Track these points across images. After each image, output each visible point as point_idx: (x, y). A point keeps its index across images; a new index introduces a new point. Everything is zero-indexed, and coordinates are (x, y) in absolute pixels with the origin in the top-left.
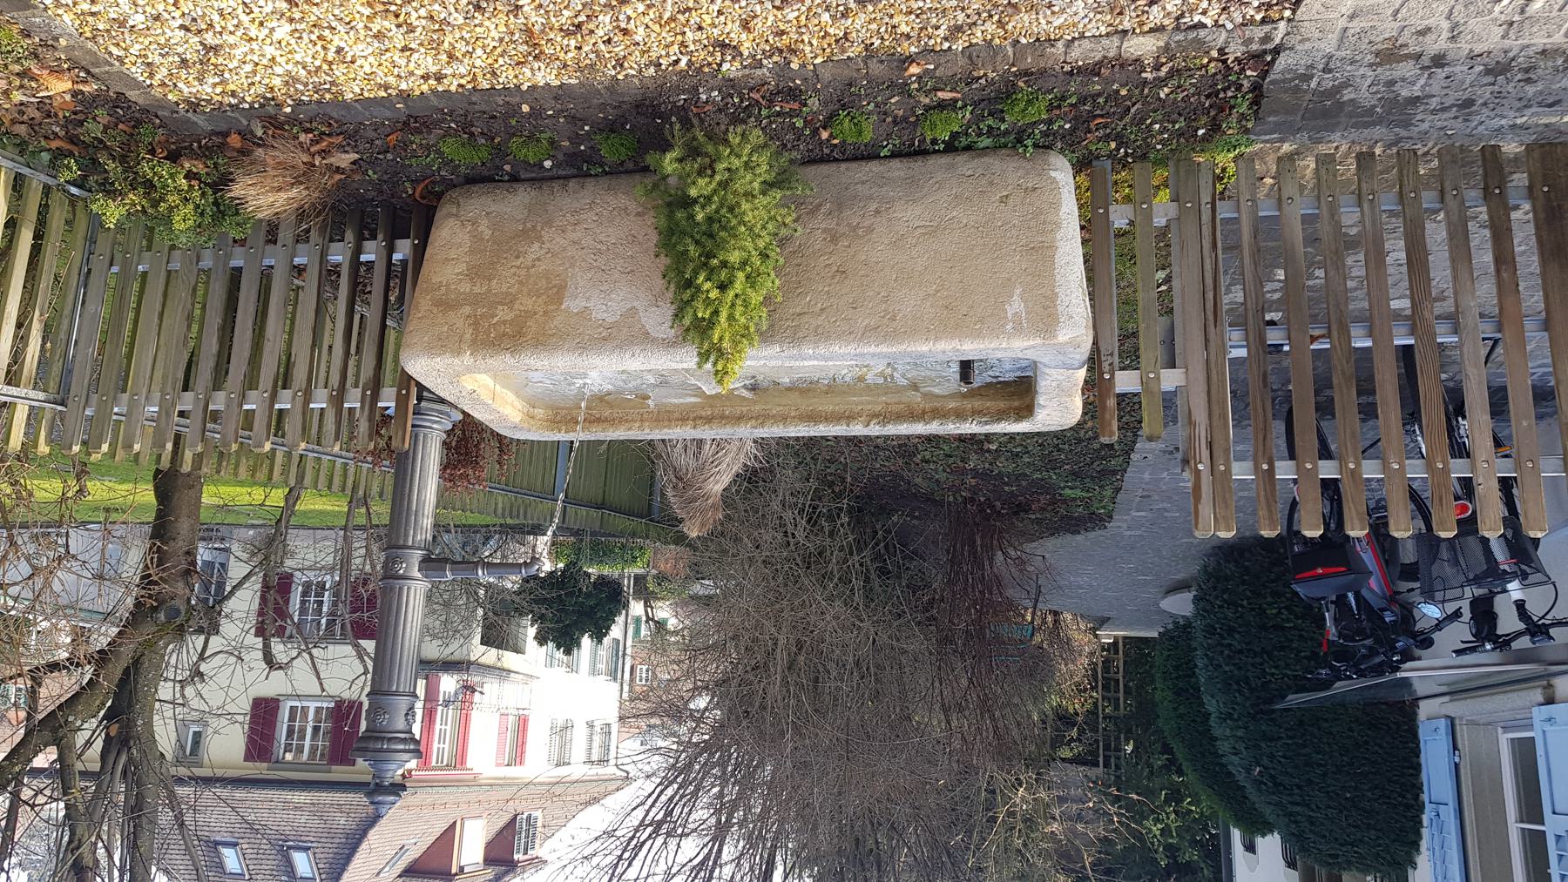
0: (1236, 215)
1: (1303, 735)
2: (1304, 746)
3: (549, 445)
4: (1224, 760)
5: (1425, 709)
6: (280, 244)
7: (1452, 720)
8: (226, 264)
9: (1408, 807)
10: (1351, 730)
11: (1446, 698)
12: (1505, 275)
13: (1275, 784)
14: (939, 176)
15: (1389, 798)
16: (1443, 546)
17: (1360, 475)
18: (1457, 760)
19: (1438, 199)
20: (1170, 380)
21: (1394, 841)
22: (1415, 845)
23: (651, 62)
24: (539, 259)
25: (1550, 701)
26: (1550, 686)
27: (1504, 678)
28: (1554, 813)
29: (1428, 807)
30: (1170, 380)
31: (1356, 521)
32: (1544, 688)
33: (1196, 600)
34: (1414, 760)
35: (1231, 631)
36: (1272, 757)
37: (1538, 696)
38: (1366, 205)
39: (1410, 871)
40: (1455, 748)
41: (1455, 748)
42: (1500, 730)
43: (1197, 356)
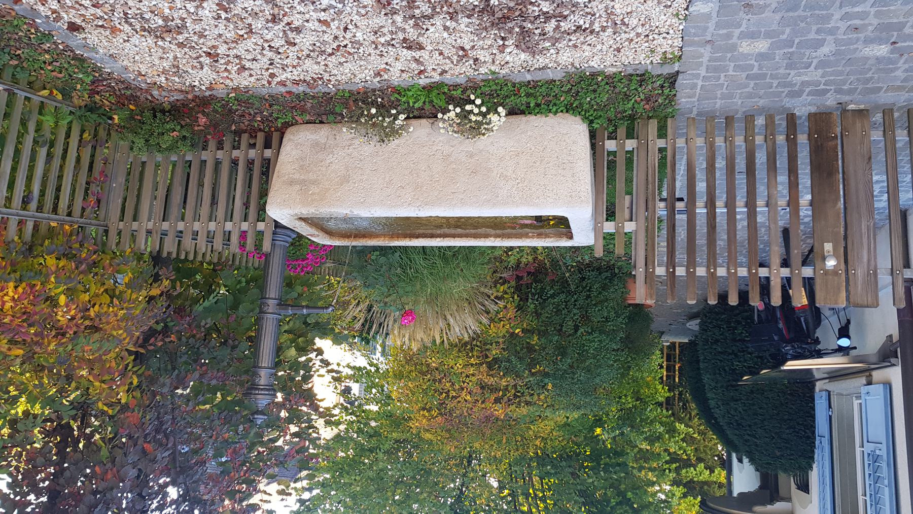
0: (666, 146)
1: (753, 399)
2: (754, 405)
3: (336, 248)
4: (713, 411)
5: (819, 385)
6: (209, 150)
7: (829, 392)
8: (183, 159)
9: (808, 437)
10: (778, 396)
11: (827, 381)
12: (792, 178)
13: (738, 425)
14: (522, 126)
15: (798, 433)
16: (31, 416)
17: (716, 275)
18: (830, 413)
19: (764, 139)
20: (629, 227)
21: (800, 456)
22: (812, 458)
23: (452, 16)
24: (331, 163)
25: (869, 383)
26: (871, 375)
27: (854, 371)
28: (868, 442)
29: (817, 438)
30: (629, 227)
31: (712, 297)
32: (867, 376)
33: (700, 324)
34: (812, 412)
35: (717, 341)
36: (736, 410)
37: (863, 380)
38: (728, 143)
39: (810, 471)
40: (830, 407)
41: (830, 407)
42: (854, 398)
43: (642, 214)
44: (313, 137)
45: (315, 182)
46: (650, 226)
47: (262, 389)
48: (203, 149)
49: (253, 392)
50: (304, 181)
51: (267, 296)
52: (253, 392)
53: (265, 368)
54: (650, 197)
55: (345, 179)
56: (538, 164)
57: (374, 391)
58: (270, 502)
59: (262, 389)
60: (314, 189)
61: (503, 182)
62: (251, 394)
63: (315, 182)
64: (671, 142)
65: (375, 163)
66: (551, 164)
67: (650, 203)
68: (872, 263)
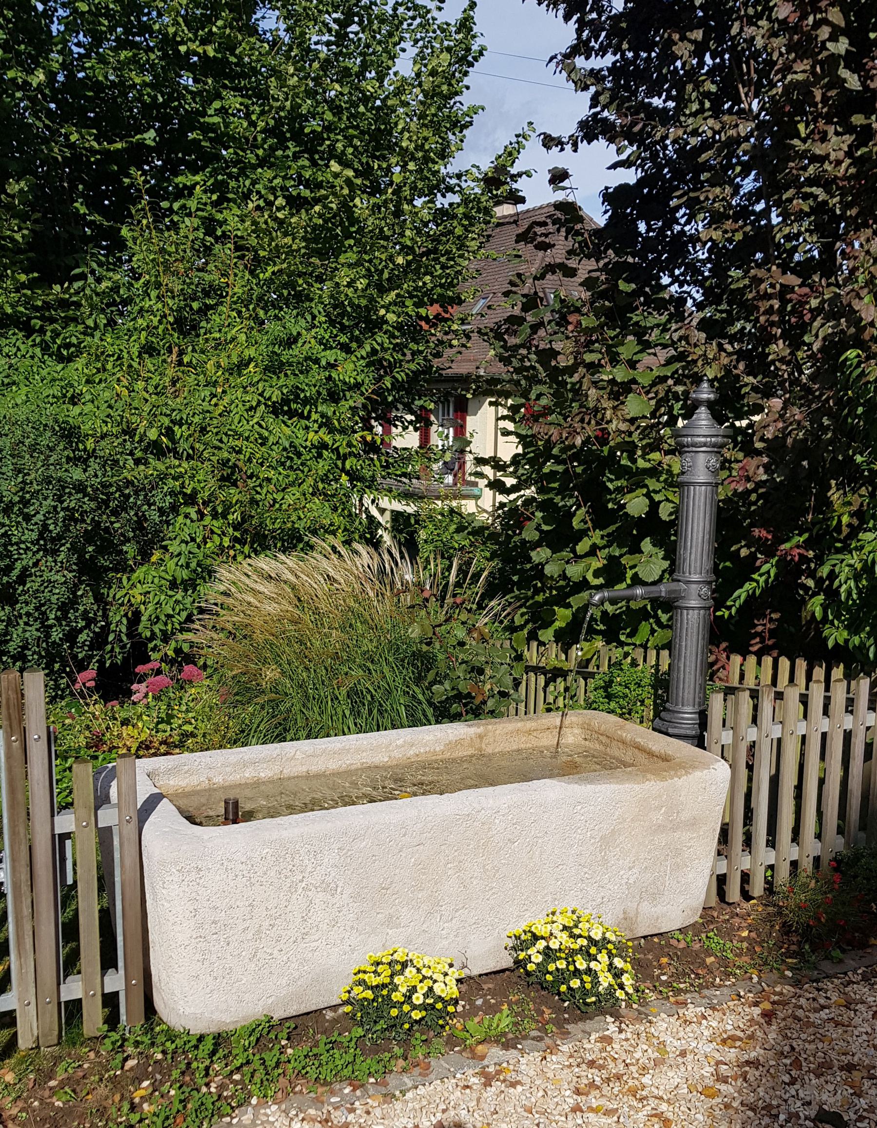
24: (630, 869)
44: (659, 910)
45: (659, 829)
46: (22, 830)
47: (705, 445)
48: (819, 857)
49: (720, 439)
50: (674, 829)
51: (702, 612)
52: (720, 439)
53: (701, 484)
54: (25, 889)
55: (607, 841)
56: (266, 924)
57: (119, 30)
58: (824, 735)
59: (705, 445)
60: (658, 817)
61: (329, 879)
62: (724, 436)
63: (659, 829)
64: (49, 998)
65: (557, 880)
66: (241, 928)
67: (24, 876)
68: (20, 797)
